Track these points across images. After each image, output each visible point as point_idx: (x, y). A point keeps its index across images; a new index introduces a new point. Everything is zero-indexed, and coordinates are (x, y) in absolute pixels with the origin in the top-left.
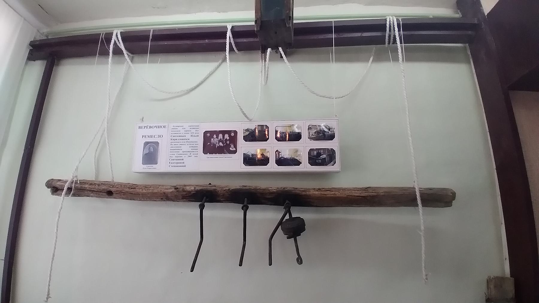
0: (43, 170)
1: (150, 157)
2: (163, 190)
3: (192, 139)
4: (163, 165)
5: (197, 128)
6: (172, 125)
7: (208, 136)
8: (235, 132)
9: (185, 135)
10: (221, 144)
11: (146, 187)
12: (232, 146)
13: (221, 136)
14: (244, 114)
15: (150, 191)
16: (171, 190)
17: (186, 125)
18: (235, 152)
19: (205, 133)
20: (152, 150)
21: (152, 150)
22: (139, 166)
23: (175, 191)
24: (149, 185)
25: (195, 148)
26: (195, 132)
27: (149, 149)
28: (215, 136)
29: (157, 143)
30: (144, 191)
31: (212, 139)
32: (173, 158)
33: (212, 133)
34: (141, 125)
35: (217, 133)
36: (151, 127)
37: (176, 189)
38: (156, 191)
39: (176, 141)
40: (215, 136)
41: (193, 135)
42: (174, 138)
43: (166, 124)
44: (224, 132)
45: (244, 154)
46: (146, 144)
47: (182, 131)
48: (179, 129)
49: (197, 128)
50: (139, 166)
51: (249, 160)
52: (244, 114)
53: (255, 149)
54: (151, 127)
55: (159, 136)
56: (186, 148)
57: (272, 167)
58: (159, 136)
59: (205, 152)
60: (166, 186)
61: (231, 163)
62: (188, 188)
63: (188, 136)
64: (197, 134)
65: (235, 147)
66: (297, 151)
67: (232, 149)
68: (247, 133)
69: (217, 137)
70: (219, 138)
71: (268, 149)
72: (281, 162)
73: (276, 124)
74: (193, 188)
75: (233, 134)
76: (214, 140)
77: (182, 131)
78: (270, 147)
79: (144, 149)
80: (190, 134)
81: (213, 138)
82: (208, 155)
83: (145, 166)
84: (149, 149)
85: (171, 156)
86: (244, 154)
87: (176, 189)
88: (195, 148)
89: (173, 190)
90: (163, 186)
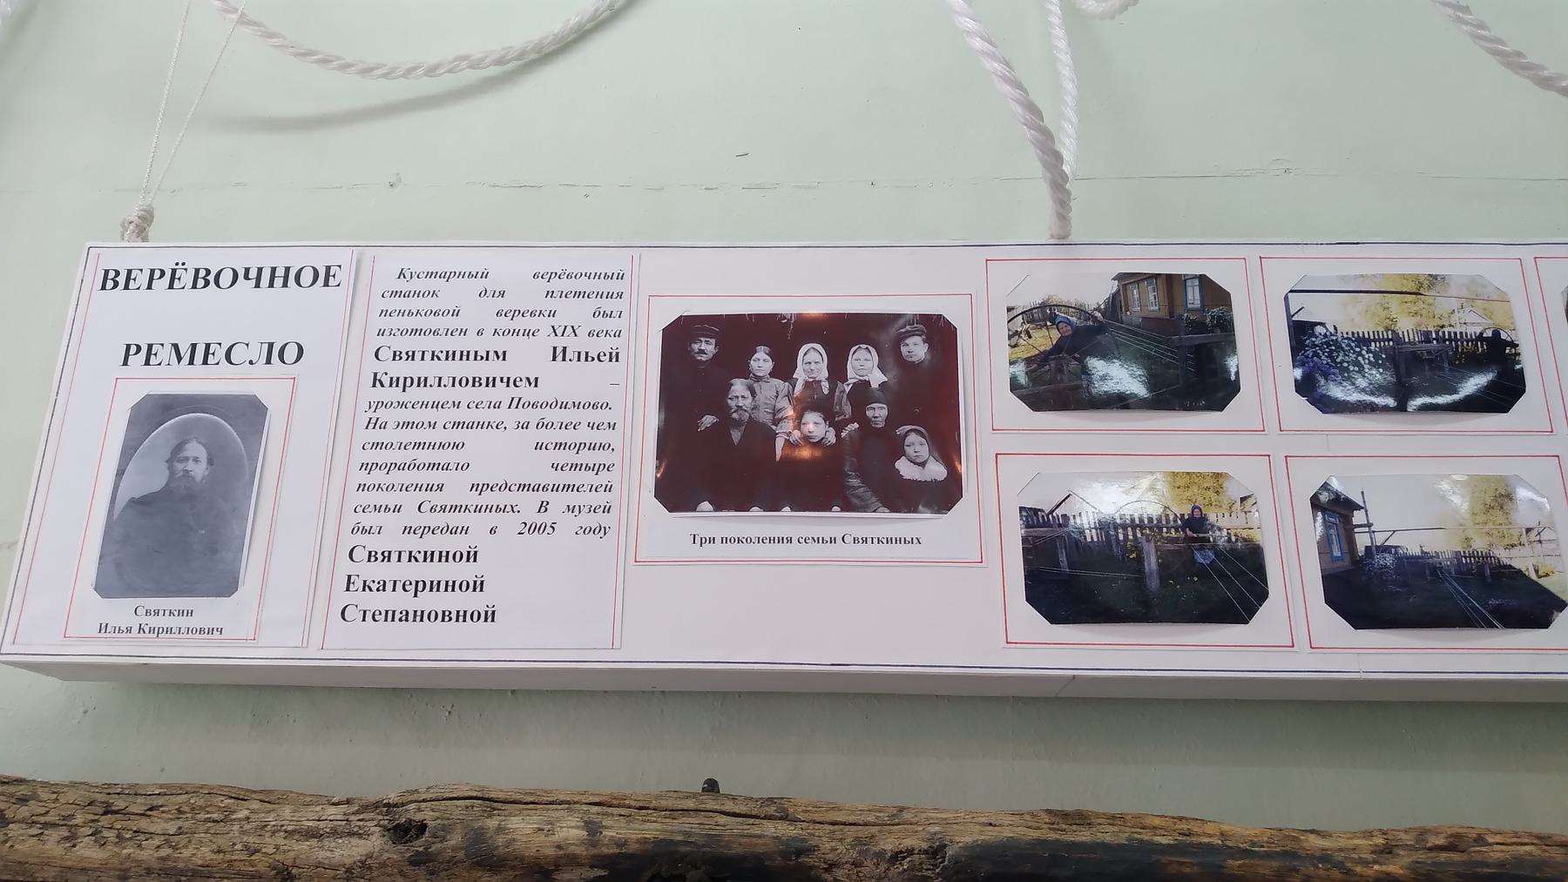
0: (636, 253)
1: (177, 526)
2: (269, 843)
3: (562, 381)
4: (281, 608)
5: (605, 290)
6: (387, 265)
7: (703, 361)
8: (940, 332)
9: (499, 344)
10: (815, 425)
11: (108, 806)
12: (917, 444)
13: (812, 361)
14: (1515, 62)
15: (148, 853)
16: (348, 851)
17: (515, 272)
18: (944, 495)
19: (680, 334)
20: (199, 470)
21: (199, 470)
22: (66, 608)
23: (396, 853)
24: (134, 791)
25: (586, 457)
26: (587, 323)
27: (176, 455)
28: (762, 361)
29: (249, 413)
30: (88, 851)
31: (739, 387)
32: (377, 544)
33: (741, 335)
34: (120, 261)
35: (781, 335)
36: (205, 278)
37: (404, 832)
38: (198, 853)
39: (414, 393)
40: (762, 361)
41: (574, 345)
42: (402, 369)
43: (340, 257)
44: (840, 333)
45: (1031, 516)
46: (155, 412)
47: (478, 313)
48: (452, 294)
49: (605, 290)
50: (66, 608)
51: (1071, 575)
52: (1515, 62)
53: (1118, 478)
54: (205, 278)
55: (274, 353)
56: (503, 453)
57: (1296, 634)
58: (274, 353)
59: (676, 492)
60: (305, 801)
61: (914, 596)
62: (523, 831)
63: (527, 357)
64: (605, 344)
65: (947, 445)
66: (1500, 498)
67: (918, 463)
68: (1044, 339)
69: (784, 369)
70: (800, 375)
71: (1245, 476)
72: (1370, 589)
73: (1284, 273)
74: (570, 831)
75: (917, 349)
76: (757, 393)
77: (478, 313)
78: (1266, 458)
79: (128, 452)
80: (545, 342)
81: (745, 373)
82: (707, 520)
83: (122, 611)
84: (176, 455)
85: (368, 520)
86: (1031, 516)
87: (404, 832)
88: (586, 457)
89: (375, 843)
90: (271, 799)
